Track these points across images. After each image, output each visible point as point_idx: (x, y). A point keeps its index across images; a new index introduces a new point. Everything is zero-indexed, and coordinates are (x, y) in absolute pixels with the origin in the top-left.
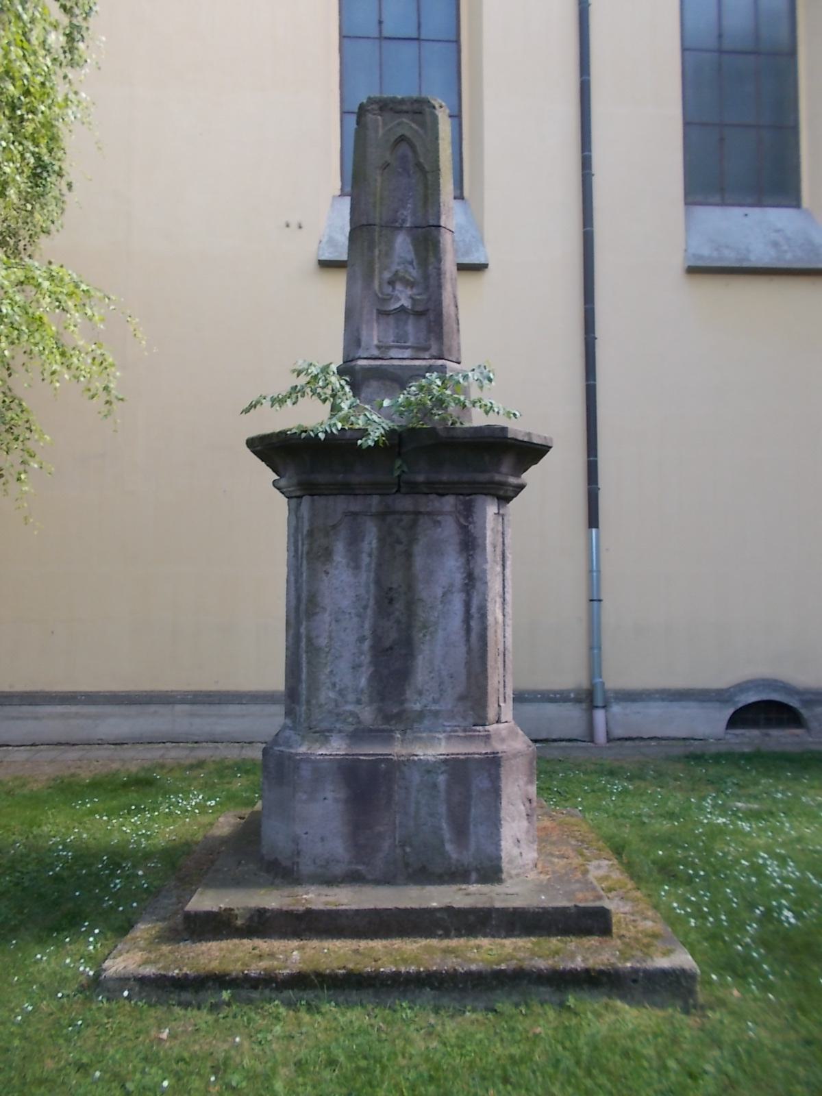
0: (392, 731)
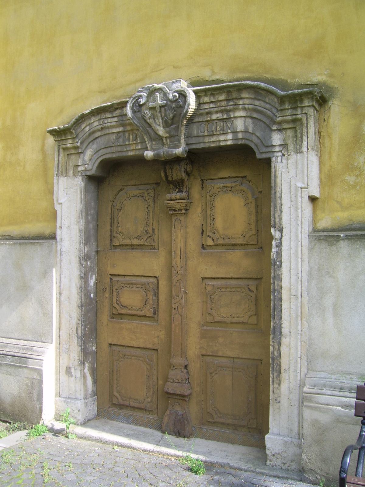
0: (113, 350)
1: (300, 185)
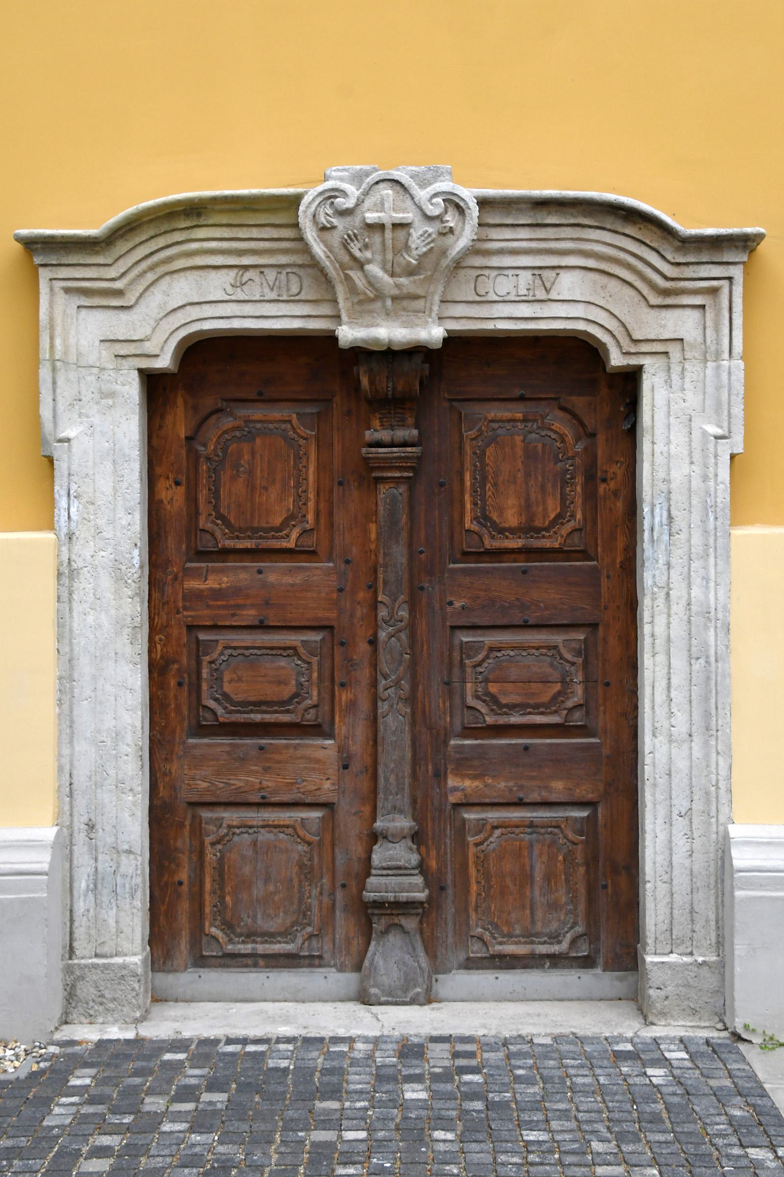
1: (713, 430)
